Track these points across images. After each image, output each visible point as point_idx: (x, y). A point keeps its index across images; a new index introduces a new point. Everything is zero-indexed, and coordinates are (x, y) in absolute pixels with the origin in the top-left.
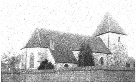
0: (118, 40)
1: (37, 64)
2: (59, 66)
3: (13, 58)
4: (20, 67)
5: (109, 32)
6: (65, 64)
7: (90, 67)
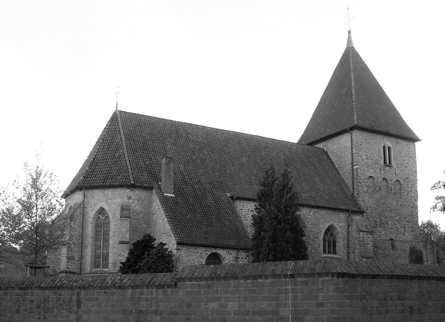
0: (385, 162)
1: (118, 254)
2: (192, 259)
3: (39, 228)
4: (63, 264)
5: (352, 128)
6: (209, 253)
7: (291, 264)
